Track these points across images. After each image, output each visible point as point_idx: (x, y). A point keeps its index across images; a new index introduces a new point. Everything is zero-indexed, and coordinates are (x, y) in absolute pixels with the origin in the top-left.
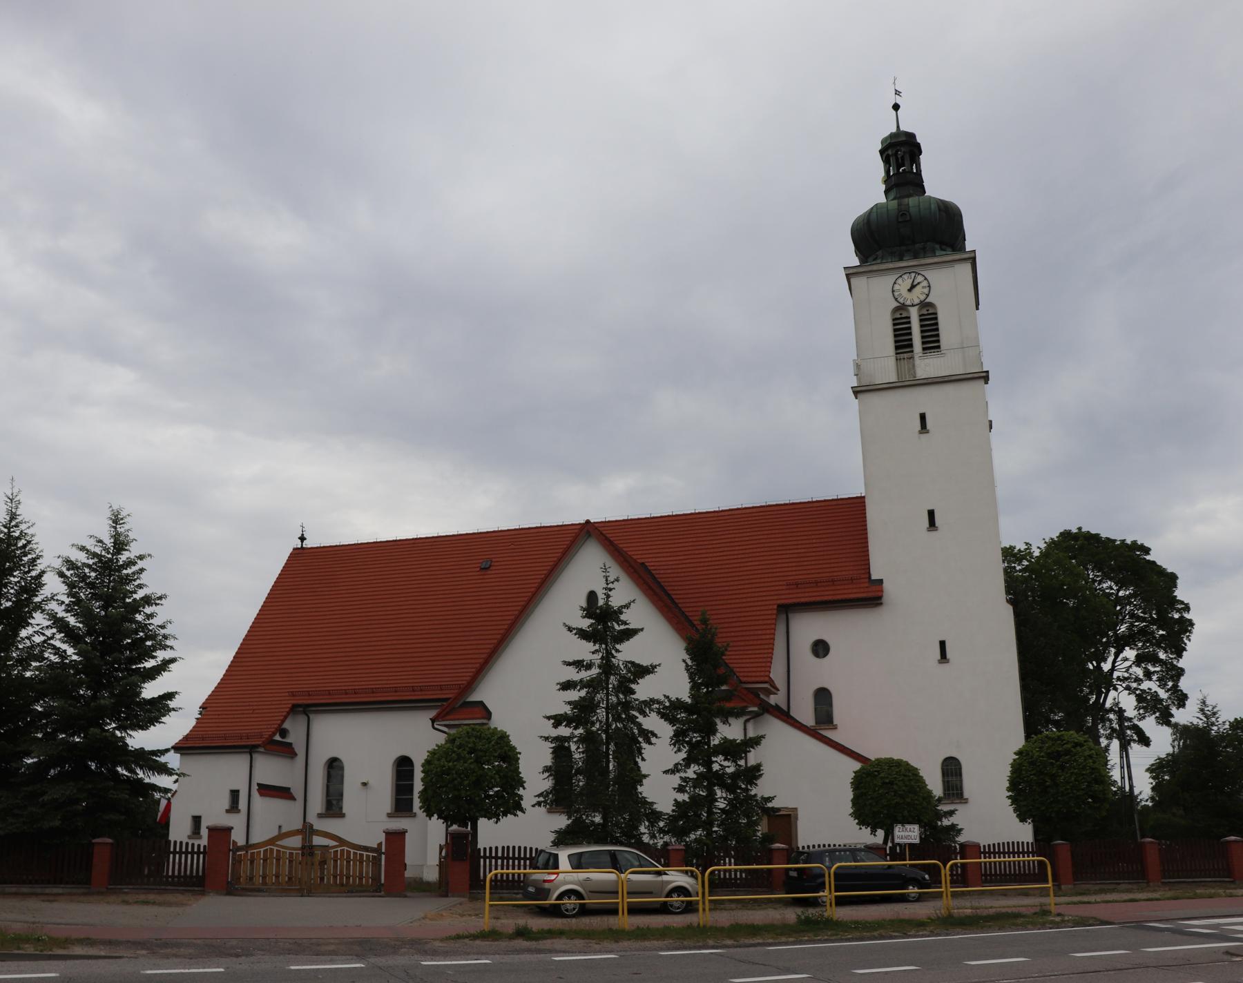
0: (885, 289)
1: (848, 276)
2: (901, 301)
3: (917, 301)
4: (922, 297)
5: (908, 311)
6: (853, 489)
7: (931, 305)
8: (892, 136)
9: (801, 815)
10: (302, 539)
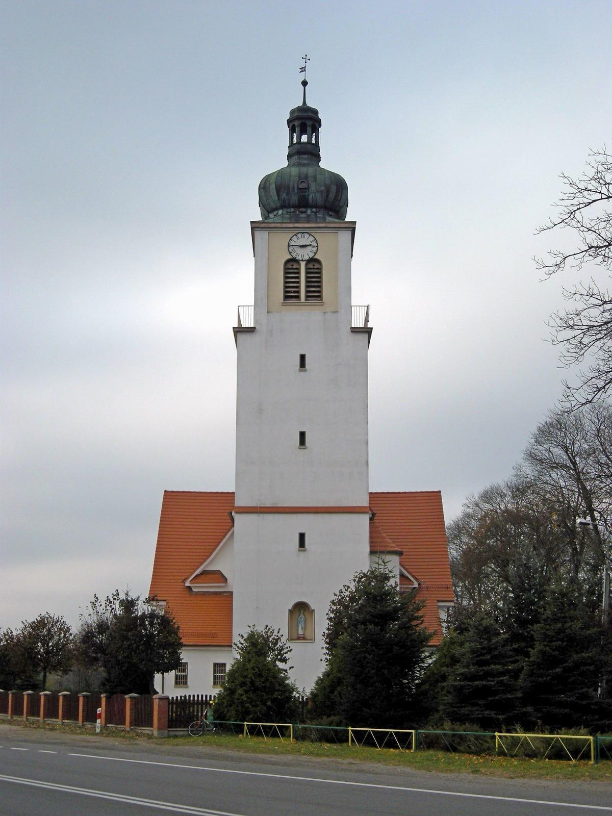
0: (282, 245)
1: (253, 229)
2: (294, 255)
3: (306, 258)
4: (311, 255)
5: (299, 264)
6: (231, 489)
7: (318, 261)
8: (299, 109)
9: (301, 430)
10: (127, 594)
